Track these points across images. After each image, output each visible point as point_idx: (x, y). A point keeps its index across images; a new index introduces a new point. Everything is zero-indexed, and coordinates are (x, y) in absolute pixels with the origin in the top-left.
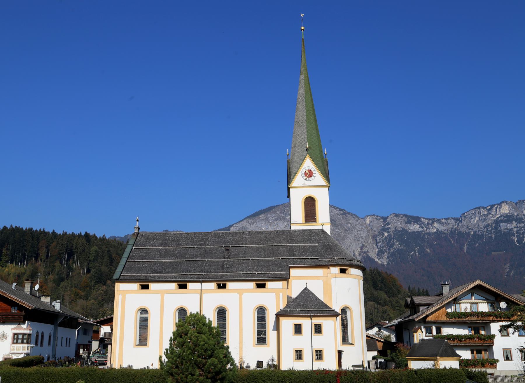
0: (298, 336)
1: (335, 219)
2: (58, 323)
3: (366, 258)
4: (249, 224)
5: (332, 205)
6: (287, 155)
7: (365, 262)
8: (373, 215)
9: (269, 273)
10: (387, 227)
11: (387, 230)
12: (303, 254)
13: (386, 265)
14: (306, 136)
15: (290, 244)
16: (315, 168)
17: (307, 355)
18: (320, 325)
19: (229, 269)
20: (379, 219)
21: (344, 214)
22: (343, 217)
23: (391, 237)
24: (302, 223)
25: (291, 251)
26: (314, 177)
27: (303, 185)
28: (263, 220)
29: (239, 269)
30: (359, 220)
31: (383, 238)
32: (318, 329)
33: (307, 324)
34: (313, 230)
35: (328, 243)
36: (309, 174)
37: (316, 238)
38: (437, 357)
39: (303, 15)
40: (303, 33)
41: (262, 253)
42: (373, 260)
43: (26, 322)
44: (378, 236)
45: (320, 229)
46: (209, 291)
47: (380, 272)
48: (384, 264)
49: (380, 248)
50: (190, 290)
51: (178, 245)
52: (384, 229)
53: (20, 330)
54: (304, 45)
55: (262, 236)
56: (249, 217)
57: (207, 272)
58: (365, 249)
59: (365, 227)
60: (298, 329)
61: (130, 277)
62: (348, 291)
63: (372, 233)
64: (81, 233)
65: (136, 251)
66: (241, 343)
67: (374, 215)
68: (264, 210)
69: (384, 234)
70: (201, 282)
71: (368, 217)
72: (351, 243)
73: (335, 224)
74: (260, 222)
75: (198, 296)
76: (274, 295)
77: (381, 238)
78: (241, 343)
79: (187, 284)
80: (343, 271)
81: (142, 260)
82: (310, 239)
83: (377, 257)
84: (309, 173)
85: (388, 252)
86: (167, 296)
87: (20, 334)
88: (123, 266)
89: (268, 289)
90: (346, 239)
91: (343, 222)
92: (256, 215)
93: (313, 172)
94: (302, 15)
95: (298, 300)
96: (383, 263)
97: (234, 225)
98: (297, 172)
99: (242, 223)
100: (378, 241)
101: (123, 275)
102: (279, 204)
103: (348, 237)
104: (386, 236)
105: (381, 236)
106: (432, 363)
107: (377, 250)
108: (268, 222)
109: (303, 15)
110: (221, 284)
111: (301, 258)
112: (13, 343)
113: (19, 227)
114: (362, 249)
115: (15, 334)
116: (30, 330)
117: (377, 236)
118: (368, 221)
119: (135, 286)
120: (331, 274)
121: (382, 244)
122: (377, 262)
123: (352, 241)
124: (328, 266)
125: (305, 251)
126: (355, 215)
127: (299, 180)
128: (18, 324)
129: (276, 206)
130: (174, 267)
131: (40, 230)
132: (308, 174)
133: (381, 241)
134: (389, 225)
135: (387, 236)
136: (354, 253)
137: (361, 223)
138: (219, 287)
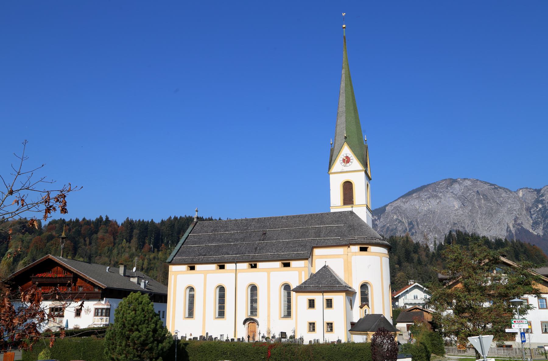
0: (312, 310)
1: (487, 194)
3: (520, 229)
4: (403, 203)
5: (483, 181)
6: (331, 144)
7: (519, 233)
8: (526, 188)
9: (293, 253)
10: (541, 199)
11: (542, 202)
12: (328, 235)
13: (542, 236)
14: (345, 125)
15: (319, 226)
16: (352, 154)
17: (319, 327)
18: (331, 300)
19: (261, 251)
20: (532, 192)
21: (495, 188)
22: (494, 192)
23: (546, 208)
24: (340, 205)
25: (318, 233)
26: (352, 162)
27: (341, 170)
28: (416, 198)
29: (270, 250)
30: (512, 193)
31: (537, 210)
32: (329, 304)
33: (319, 299)
34: (343, 212)
35: (354, 223)
36: (347, 160)
37: (344, 219)
38: (367, 332)
39: (345, 14)
40: (344, 31)
41: (292, 235)
42: (528, 231)
43: (104, 298)
44: (532, 208)
45: (349, 211)
46: (243, 271)
47: (522, 243)
48: (540, 235)
49: (535, 220)
50: (293, 267)
51: (225, 231)
52: (537, 201)
53: (99, 305)
54: (345, 42)
55: (297, 219)
56: (403, 197)
57: (242, 254)
58: (519, 221)
59: (518, 201)
60: (312, 304)
61: (180, 260)
62: (368, 268)
63: (525, 206)
65: (191, 237)
66: (269, 316)
67: (527, 188)
68: (416, 189)
69: (538, 206)
70: (236, 263)
71: (521, 190)
72: (504, 216)
73: (487, 199)
74: (414, 201)
77: (536, 210)
78: (269, 316)
79: (224, 265)
80: (363, 249)
81: (194, 245)
82: (338, 221)
83: (532, 229)
84: (346, 160)
85: (543, 223)
86: (209, 276)
87: (100, 309)
88: (177, 250)
89: (226, 270)
90: (499, 212)
91: (495, 197)
92: (410, 194)
93: (351, 158)
94: (343, 15)
95: (315, 277)
96: (539, 233)
97: (390, 205)
98: (335, 159)
99: (396, 202)
100: (532, 213)
102: (430, 183)
103: (500, 211)
104: (540, 208)
105: (535, 208)
106: (365, 337)
107: (532, 222)
108: (421, 200)
109: (345, 14)
110: (253, 264)
111: (325, 238)
112: (95, 316)
113: (192, 217)
114: (515, 221)
115: (96, 309)
116: (107, 305)
117: (531, 208)
118: (521, 194)
119: (184, 268)
120: (351, 252)
121: (536, 216)
122: (532, 233)
123: (505, 214)
124: (348, 245)
125: (330, 232)
126: (506, 189)
127: (338, 166)
128: (99, 300)
129: (428, 185)
130: (217, 250)
131: (139, 220)
132: (346, 161)
133: (535, 213)
134: (543, 196)
135: (542, 207)
136: (507, 225)
137: (513, 197)
138: (252, 267)
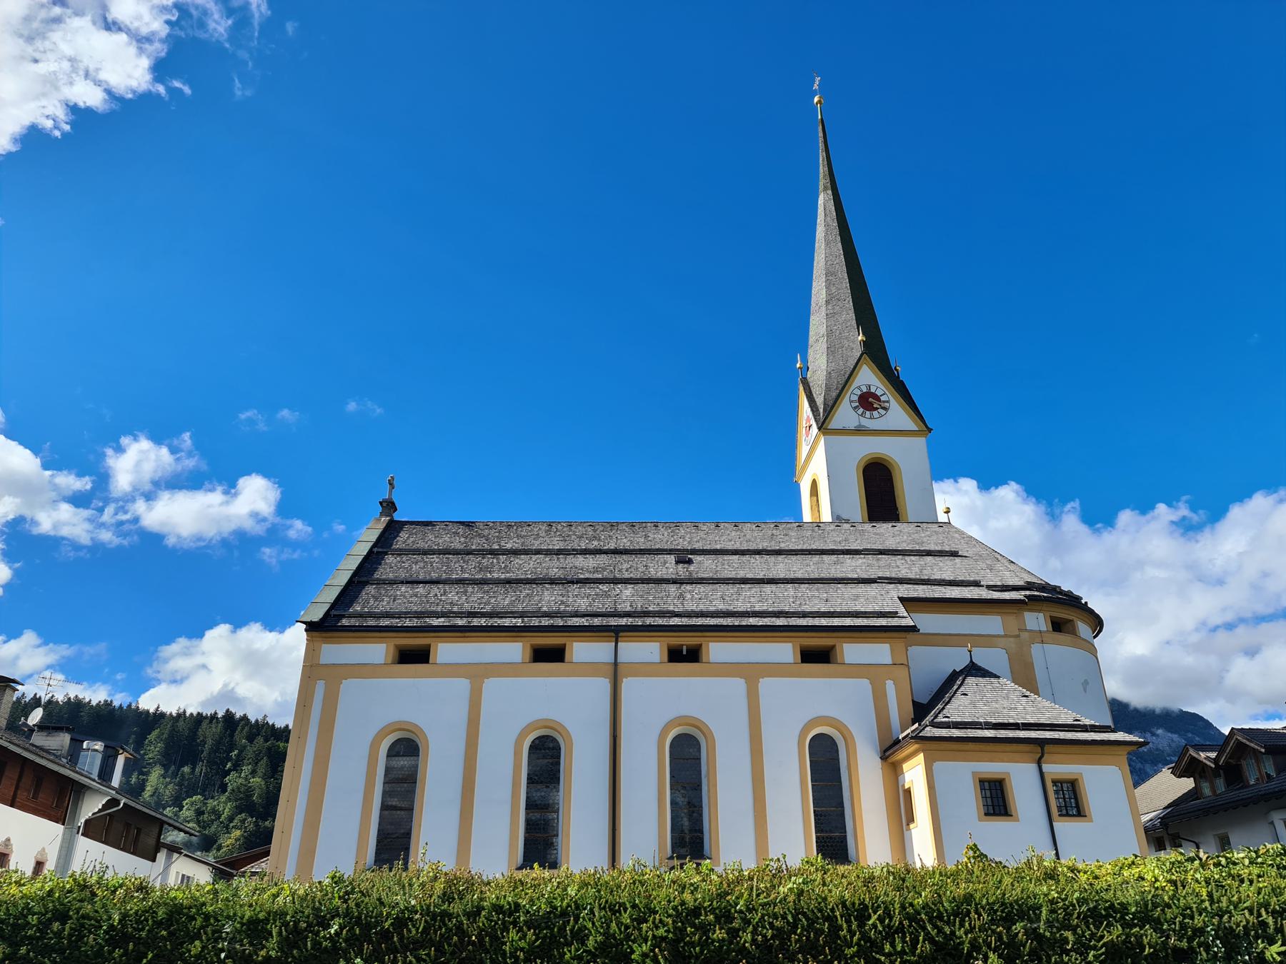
2: (83, 821)
16: (884, 390)
46: (643, 669)
62: (1085, 690)
64: (216, 713)
75: (604, 684)
76: (865, 683)
101: (336, 613)
138: (675, 655)
